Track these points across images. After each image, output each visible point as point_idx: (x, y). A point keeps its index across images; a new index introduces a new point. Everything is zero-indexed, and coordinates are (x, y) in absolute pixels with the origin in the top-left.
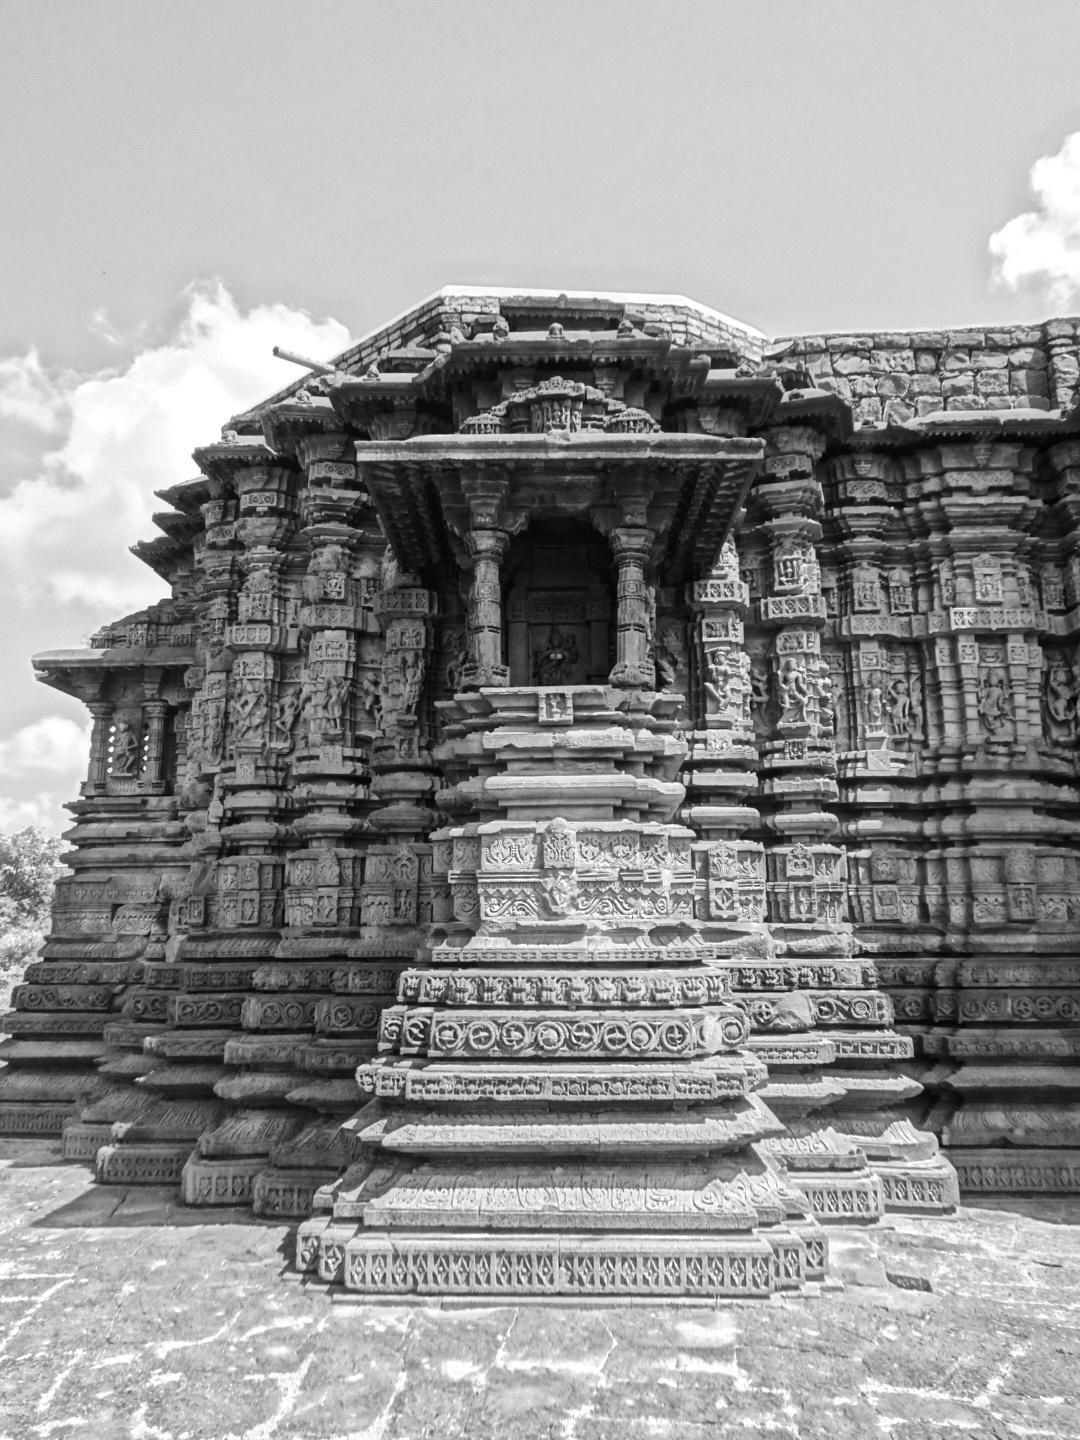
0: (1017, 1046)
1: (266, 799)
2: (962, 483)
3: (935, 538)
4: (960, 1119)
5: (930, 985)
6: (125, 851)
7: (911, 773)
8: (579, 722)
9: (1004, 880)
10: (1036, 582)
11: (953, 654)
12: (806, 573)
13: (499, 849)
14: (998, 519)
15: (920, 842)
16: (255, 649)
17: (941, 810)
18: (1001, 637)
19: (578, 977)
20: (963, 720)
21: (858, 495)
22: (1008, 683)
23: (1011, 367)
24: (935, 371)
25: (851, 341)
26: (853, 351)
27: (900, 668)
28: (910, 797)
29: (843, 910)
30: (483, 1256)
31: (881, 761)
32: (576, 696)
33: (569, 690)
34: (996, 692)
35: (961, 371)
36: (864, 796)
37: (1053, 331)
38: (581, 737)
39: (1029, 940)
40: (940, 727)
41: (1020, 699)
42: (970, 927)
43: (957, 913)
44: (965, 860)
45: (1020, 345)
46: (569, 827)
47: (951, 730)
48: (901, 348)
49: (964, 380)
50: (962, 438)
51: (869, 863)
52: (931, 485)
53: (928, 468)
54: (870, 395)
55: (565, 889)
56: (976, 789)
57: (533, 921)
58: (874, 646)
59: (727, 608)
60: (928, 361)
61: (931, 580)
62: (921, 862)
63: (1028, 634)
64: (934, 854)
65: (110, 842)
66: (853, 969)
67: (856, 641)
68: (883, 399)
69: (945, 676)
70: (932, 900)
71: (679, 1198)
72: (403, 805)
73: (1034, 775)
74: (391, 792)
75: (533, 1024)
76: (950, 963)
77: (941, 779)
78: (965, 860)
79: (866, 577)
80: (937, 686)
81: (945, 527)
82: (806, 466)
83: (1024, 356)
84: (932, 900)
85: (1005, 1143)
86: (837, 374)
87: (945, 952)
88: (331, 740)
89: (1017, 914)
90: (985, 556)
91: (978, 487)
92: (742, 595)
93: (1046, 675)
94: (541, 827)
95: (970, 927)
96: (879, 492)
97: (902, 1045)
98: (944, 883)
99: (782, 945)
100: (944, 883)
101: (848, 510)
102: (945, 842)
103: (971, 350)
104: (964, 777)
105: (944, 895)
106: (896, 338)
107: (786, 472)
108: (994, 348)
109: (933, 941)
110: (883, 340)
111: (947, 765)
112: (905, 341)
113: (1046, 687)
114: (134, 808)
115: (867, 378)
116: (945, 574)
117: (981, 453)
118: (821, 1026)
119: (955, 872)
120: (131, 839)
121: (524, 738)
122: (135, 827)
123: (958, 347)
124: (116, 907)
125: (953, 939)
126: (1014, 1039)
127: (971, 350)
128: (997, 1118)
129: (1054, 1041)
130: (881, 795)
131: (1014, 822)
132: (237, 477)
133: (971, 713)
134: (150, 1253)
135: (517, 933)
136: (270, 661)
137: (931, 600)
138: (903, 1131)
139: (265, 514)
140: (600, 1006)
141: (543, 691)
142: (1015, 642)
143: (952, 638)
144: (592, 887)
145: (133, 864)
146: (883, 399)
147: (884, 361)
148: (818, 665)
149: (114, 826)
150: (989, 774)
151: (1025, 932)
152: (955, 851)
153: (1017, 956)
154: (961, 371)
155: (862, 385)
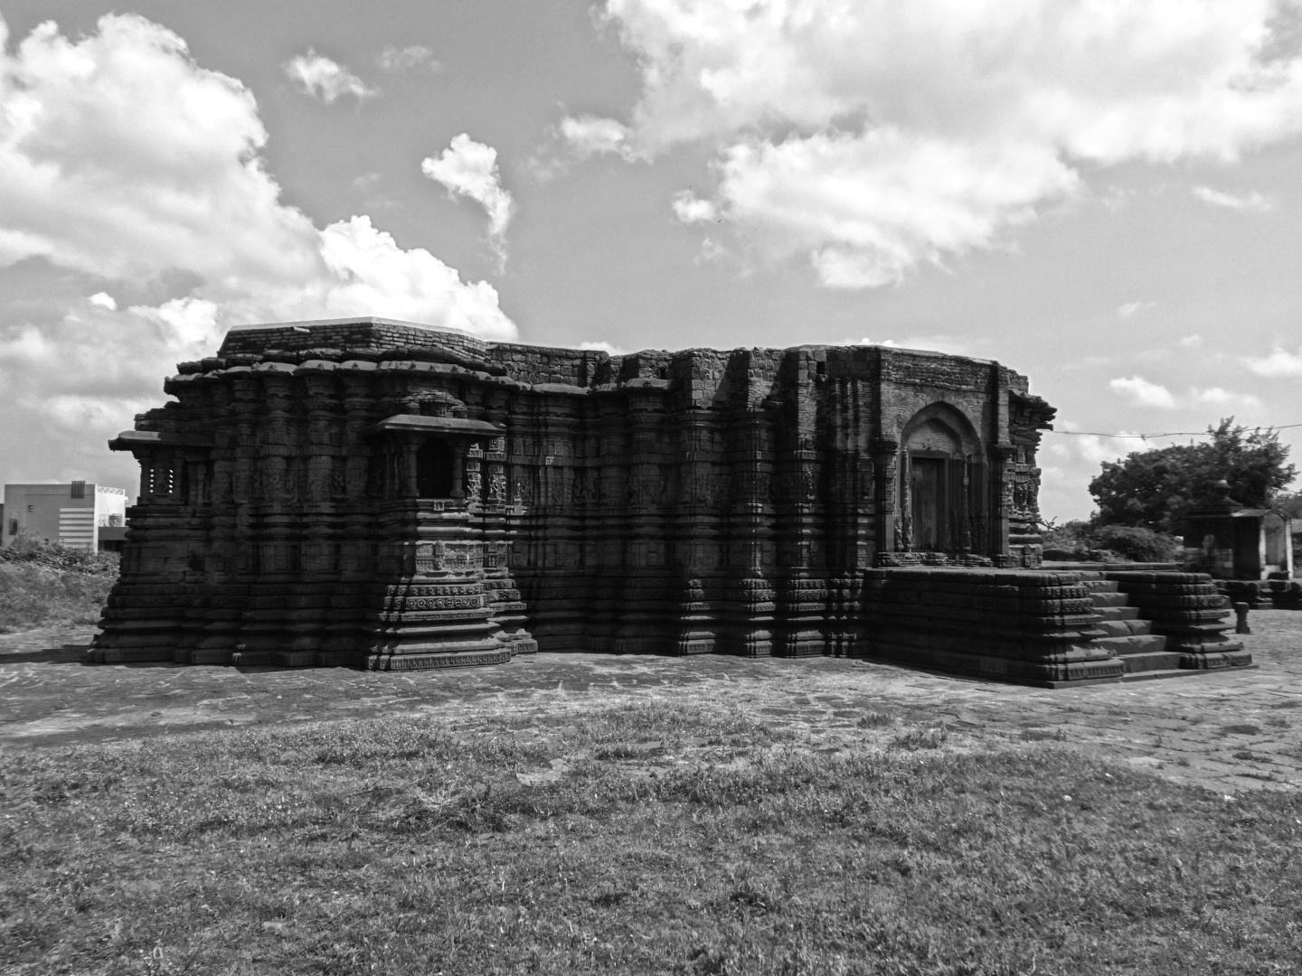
1: (285, 519)
3: (543, 430)
4: (538, 629)
5: (531, 587)
6: (170, 532)
8: (446, 511)
9: (556, 552)
10: (574, 447)
11: (546, 472)
13: (421, 549)
15: (529, 538)
16: (279, 456)
17: (537, 528)
18: (561, 468)
19: (447, 586)
20: (547, 496)
21: (517, 410)
22: (562, 484)
23: (573, 365)
24: (548, 364)
26: (519, 352)
27: (527, 475)
29: (506, 563)
30: (428, 659)
33: (443, 501)
34: (558, 487)
36: (513, 522)
37: (588, 355)
38: (446, 515)
39: (561, 572)
40: (539, 498)
41: (566, 490)
42: (544, 568)
43: (540, 563)
44: (544, 545)
45: (576, 358)
46: (443, 543)
47: (542, 499)
49: (557, 368)
52: (543, 410)
53: (543, 404)
55: (441, 562)
56: (549, 521)
57: (432, 571)
59: (474, 459)
60: (545, 360)
61: (540, 445)
62: (529, 545)
63: (570, 467)
64: (534, 542)
65: (159, 527)
66: (509, 582)
67: (513, 465)
68: (529, 373)
69: (542, 480)
70: (532, 558)
71: (476, 643)
72: (358, 527)
73: (567, 517)
75: (435, 600)
76: (537, 579)
77: (538, 517)
78: (544, 545)
79: (519, 441)
80: (539, 483)
81: (547, 426)
83: (577, 362)
84: (532, 558)
85: (550, 635)
86: (513, 361)
87: (536, 576)
88: (324, 500)
89: (559, 563)
91: (557, 414)
92: (481, 455)
93: (574, 480)
94: (434, 543)
95: (544, 568)
96: (525, 410)
97: (523, 606)
98: (537, 553)
99: (486, 575)
100: (537, 553)
102: (537, 538)
103: (560, 357)
104: (546, 516)
105: (536, 557)
108: (568, 358)
109: (532, 572)
111: (541, 512)
113: (574, 485)
116: (545, 443)
118: (500, 601)
119: (540, 550)
120: (173, 526)
121: (428, 515)
122: (174, 520)
124: (166, 558)
125: (539, 572)
127: (560, 357)
128: (548, 628)
129: (566, 603)
131: (560, 533)
133: (550, 494)
135: (428, 574)
137: (539, 451)
138: (522, 632)
139: (92, 285)
140: (453, 594)
141: (436, 501)
142: (566, 470)
143: (546, 467)
144: (449, 561)
145: (174, 538)
146: (529, 373)
147: (530, 357)
148: (503, 477)
149: (161, 520)
150: (553, 516)
152: (540, 542)
153: (557, 577)
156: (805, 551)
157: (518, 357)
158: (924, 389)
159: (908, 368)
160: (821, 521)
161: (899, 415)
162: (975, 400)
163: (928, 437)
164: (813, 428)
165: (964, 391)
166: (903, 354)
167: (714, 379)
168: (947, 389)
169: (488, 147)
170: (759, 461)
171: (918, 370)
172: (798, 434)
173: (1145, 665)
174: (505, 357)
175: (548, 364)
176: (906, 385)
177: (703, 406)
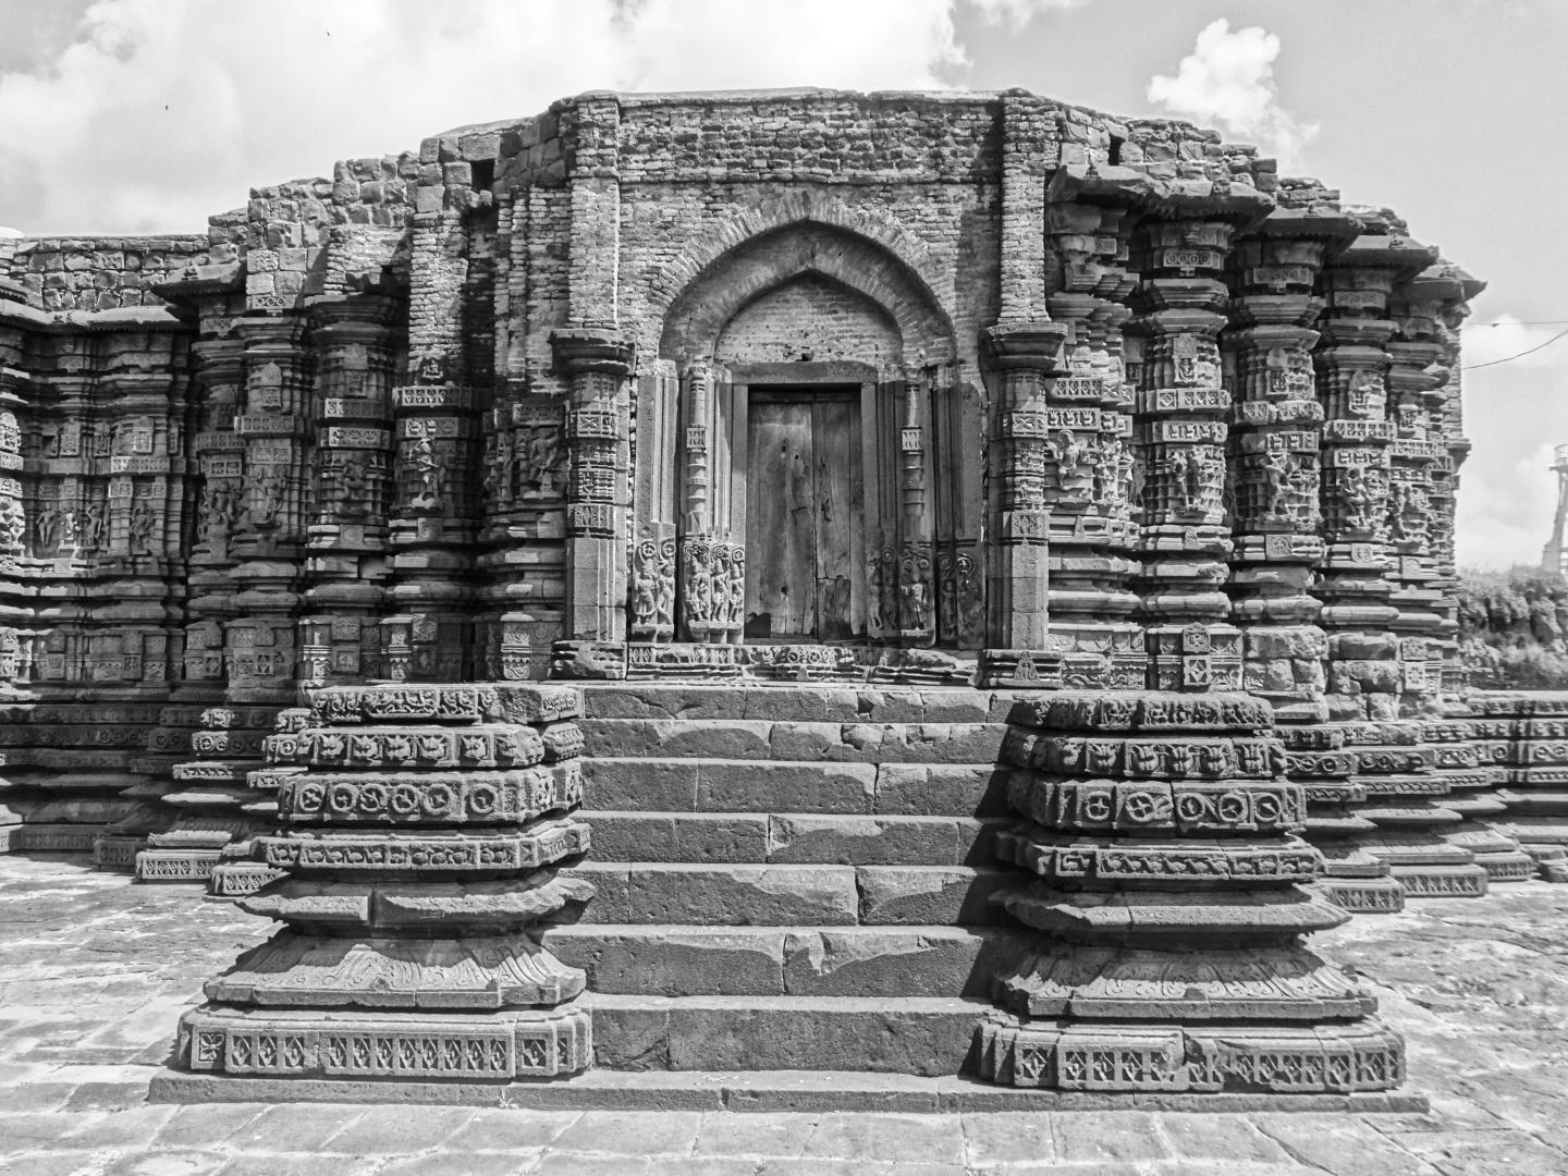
0: (89, 762)
7: (92, 574)
14: (156, 390)
21: (68, 367)
24: (138, 269)
25: (77, 244)
26: (79, 251)
28: (82, 592)
31: (65, 567)
35: (156, 270)
48: (115, 250)
51: (47, 639)
54: (88, 288)
58: (73, 482)
60: (134, 261)
62: (169, 638)
67: (107, 479)
68: (98, 290)
74: (252, 577)
82: (1309, 281)
90: (144, 418)
103: (165, 253)
106: (111, 243)
107: (1281, 284)
110: (100, 244)
112: (116, 244)
115: (87, 274)
123: (154, 251)
126: (89, 757)
127: (165, 253)
128: (73, 809)
130: (61, 591)
134: (1545, 994)
140: (392, 766)
147: (101, 260)
151: (132, 686)
154: (156, 270)
156: (398, 639)
157: (75, 262)
158: (739, 189)
159: (685, 140)
160: (450, 560)
161: (656, 270)
162: (930, 209)
163: (803, 324)
164: (451, 327)
165: (886, 185)
166: (667, 104)
167: (305, 243)
168: (820, 184)
169: (1272, 64)
170: (334, 422)
171: (703, 142)
172: (407, 347)
173: (875, 1045)
174: (51, 264)
175: (138, 269)
176: (678, 184)
177: (270, 308)
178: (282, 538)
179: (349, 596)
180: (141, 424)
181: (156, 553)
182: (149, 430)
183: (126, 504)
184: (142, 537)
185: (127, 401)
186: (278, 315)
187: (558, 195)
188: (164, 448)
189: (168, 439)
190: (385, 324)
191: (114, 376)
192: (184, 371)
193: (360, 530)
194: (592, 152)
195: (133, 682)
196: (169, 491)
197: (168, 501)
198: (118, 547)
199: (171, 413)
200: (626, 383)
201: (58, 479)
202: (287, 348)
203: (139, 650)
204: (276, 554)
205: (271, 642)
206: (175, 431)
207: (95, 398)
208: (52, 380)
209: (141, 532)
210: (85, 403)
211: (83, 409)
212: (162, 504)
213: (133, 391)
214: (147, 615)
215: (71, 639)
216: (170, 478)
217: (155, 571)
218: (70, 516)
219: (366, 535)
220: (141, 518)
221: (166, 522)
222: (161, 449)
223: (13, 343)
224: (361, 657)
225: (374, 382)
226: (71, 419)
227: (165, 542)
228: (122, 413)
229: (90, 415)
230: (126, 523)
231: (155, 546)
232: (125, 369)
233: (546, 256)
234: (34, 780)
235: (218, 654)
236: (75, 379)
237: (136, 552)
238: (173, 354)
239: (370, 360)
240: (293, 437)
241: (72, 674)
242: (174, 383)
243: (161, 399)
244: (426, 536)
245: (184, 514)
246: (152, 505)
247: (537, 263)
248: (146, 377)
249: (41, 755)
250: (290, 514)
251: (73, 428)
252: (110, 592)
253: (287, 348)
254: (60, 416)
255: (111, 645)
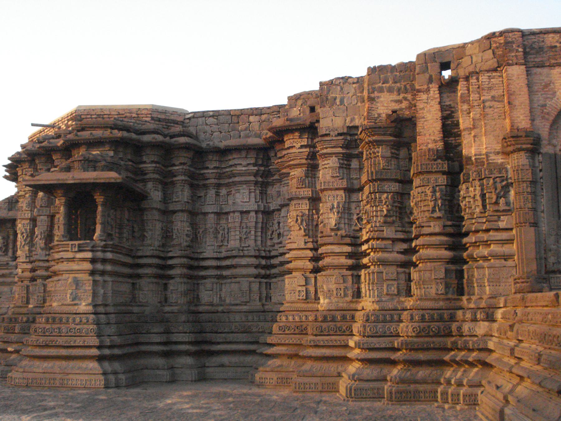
2: (238, 163)
12: (182, 195)
14: (249, 174)
28: (219, 263)
32: (79, 244)
33: (77, 243)
50: (237, 149)
58: (212, 215)
62: (260, 282)
86: (207, 124)
90: (244, 186)
101: (206, 171)
114: (4, 265)
117: (244, 154)
126: (231, 337)
128: (225, 359)
132: (36, 158)
136: (31, 222)
151: (245, 305)
155: (215, 128)
178: (344, 234)
179: (391, 259)
180: (244, 189)
181: (252, 245)
182: (247, 192)
183: (237, 225)
184: (245, 238)
185: (237, 179)
186: (336, 136)
187: (494, 74)
188: (254, 199)
189: (255, 195)
190: (395, 136)
191: (231, 169)
192: (261, 165)
193: (393, 229)
194: (513, 54)
195: (246, 303)
196: (257, 218)
197: (256, 223)
198: (234, 243)
199: (256, 183)
200: (537, 156)
201: (205, 214)
202: (340, 150)
203: (247, 289)
204: (342, 242)
205: (304, 284)
206: (258, 192)
207: (220, 179)
208: (202, 172)
209: (245, 236)
210: (216, 181)
211: (216, 184)
212: (254, 224)
213: (240, 175)
214: (250, 273)
215: (215, 285)
216: (256, 212)
217: (253, 253)
218: (211, 230)
219: (396, 231)
220: (244, 230)
221: (255, 232)
222: (253, 200)
223: (189, 156)
224: (398, 287)
225: (393, 163)
226: (211, 188)
227: (256, 241)
228: (235, 183)
229: (218, 186)
230: (238, 233)
231: (251, 242)
232: (235, 165)
233: (491, 101)
234: (206, 347)
235: (304, 288)
236: (214, 171)
237: (243, 245)
238: (256, 159)
239: (392, 153)
240: (344, 189)
241: (216, 300)
242: (258, 171)
243: (252, 178)
244: (437, 230)
245: (262, 228)
246: (249, 224)
247: (487, 104)
248: (246, 168)
249: (208, 336)
250: (345, 224)
251: (212, 192)
252: (234, 263)
253: (340, 150)
254: (205, 186)
255: (235, 287)
